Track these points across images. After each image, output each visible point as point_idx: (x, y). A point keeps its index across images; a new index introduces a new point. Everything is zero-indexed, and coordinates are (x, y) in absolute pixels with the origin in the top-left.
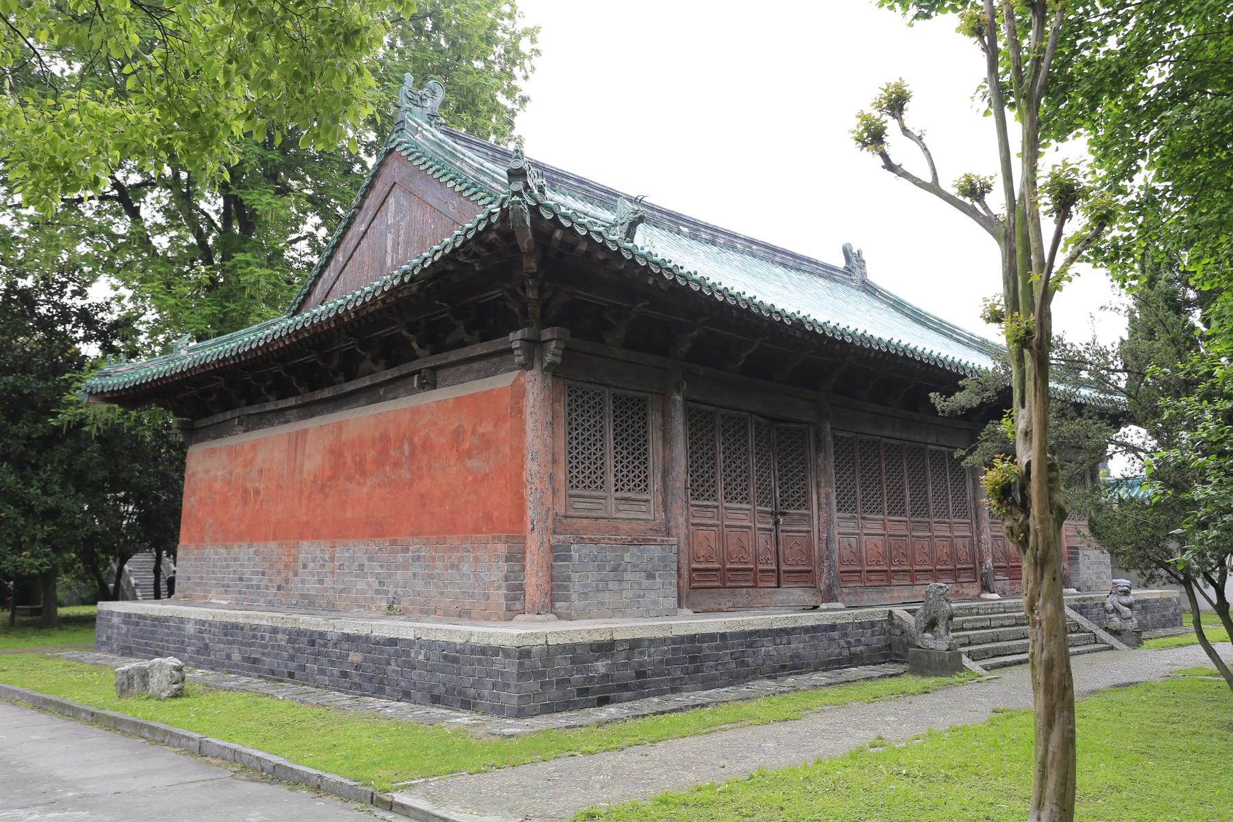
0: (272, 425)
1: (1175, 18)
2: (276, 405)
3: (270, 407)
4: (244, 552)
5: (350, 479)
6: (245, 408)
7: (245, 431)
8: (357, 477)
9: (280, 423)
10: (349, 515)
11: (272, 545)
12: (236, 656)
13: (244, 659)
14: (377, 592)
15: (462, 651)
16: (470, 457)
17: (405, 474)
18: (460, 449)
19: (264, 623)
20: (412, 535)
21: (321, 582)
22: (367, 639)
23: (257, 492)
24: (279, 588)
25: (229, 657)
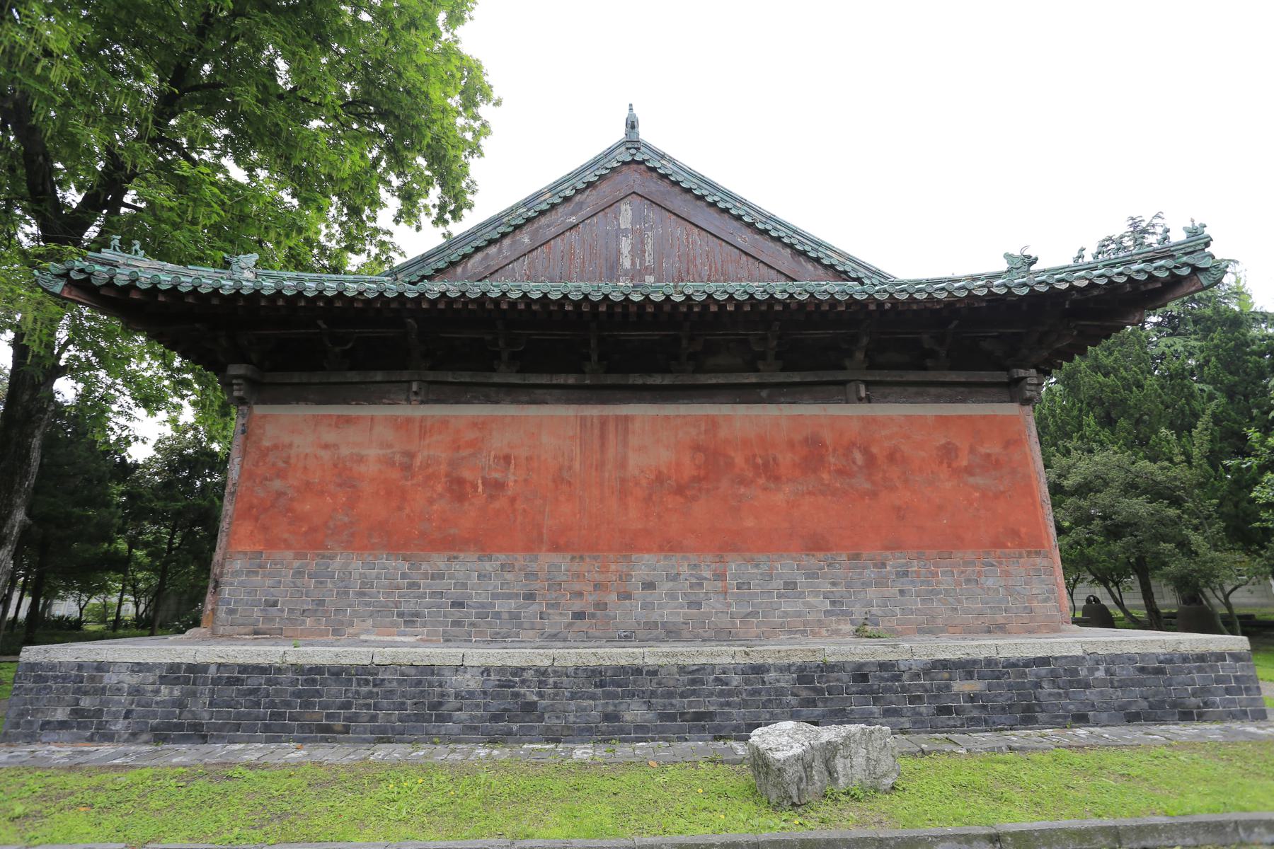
1: (349, 133)
3: (497, 379)
7: (422, 402)
15: (1170, 661)
16: (972, 474)
18: (954, 465)
22: (990, 662)
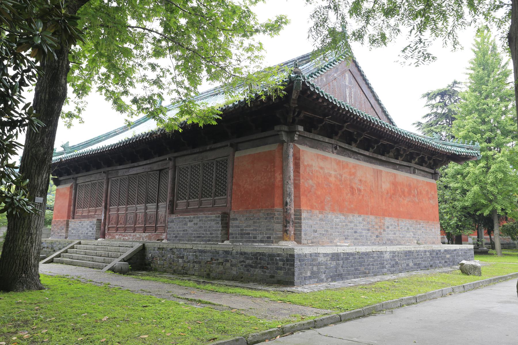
0: (351, 157)
2: (359, 150)
4: (357, 219)
5: (400, 196)
6: (425, 168)
8: (403, 196)
9: (354, 158)
10: (401, 209)
11: (372, 217)
12: (411, 264)
13: (415, 264)
19: (421, 249)
20: (420, 219)
21: (395, 234)
23: (360, 190)
24: (377, 236)
25: (408, 265)
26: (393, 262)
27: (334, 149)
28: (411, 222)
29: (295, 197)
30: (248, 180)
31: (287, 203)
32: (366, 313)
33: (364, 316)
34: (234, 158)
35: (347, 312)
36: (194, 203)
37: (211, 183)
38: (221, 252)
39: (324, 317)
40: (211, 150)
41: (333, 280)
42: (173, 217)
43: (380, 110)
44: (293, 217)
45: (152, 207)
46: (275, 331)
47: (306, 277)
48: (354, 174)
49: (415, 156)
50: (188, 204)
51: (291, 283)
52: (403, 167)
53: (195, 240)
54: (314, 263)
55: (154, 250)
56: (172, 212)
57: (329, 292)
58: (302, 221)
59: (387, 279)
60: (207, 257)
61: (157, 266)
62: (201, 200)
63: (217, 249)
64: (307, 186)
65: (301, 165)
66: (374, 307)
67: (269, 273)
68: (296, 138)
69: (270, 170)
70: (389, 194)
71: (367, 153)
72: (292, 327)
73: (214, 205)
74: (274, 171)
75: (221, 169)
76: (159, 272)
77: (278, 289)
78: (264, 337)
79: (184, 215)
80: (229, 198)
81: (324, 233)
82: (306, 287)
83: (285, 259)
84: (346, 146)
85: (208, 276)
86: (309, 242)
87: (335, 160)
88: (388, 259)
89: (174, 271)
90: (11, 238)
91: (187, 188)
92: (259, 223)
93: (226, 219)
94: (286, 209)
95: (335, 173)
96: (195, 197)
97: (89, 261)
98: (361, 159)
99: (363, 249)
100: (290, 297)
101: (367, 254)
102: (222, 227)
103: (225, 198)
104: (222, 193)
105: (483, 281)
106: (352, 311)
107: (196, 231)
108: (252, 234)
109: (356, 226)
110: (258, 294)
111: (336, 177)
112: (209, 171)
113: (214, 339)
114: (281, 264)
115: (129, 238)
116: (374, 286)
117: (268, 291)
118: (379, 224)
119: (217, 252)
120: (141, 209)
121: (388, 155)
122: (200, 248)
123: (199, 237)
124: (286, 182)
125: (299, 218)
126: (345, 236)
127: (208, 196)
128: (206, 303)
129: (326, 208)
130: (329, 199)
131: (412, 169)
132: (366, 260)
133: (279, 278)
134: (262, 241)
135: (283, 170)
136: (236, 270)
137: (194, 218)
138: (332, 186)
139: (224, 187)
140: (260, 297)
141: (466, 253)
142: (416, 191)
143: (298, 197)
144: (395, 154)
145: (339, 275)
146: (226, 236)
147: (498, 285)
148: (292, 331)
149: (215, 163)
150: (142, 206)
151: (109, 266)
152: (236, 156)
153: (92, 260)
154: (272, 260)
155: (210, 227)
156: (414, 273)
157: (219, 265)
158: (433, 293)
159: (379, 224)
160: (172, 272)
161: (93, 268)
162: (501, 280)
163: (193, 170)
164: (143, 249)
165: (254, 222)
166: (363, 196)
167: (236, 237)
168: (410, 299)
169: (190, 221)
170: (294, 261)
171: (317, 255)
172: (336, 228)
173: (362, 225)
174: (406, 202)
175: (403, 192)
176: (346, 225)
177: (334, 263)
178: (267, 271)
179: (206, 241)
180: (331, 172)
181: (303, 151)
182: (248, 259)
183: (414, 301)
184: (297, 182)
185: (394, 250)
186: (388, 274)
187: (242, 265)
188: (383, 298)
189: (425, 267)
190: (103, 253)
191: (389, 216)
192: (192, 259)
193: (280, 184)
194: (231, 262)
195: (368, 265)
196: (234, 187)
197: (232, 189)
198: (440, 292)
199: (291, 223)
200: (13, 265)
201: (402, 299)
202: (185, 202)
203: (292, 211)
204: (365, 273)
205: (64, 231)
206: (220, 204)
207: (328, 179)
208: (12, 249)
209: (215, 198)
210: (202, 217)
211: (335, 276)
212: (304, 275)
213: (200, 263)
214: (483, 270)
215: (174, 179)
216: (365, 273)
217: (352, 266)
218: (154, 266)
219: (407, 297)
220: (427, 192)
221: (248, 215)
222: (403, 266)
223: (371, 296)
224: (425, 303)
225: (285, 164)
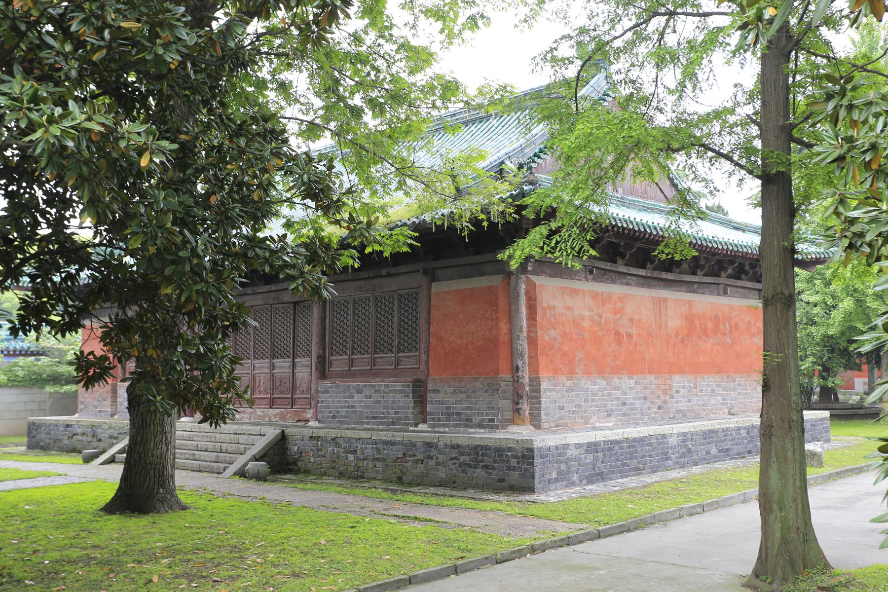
0: (615, 283)
2: (628, 270)
5: (700, 338)
8: (704, 337)
9: (621, 283)
10: (701, 359)
11: (651, 378)
12: (714, 451)
13: (720, 451)
14: (722, 404)
17: (728, 340)
19: (732, 425)
20: (735, 373)
21: (689, 401)
23: (630, 336)
24: (660, 408)
25: (708, 453)
26: (684, 450)
27: (588, 273)
28: (718, 378)
29: (530, 357)
30: (455, 331)
31: (518, 369)
32: (632, 527)
33: (629, 531)
34: (430, 292)
35: (607, 527)
36: (362, 361)
37: (390, 329)
38: (419, 445)
39: (579, 533)
40: (389, 275)
41: (590, 482)
42: (327, 384)
43: (668, 182)
44: (527, 388)
45: (283, 366)
46: (524, 549)
47: (551, 479)
48: (621, 311)
49: (725, 265)
50: (351, 363)
51: (531, 490)
52: (706, 285)
53: (368, 423)
54: (562, 458)
55: (302, 440)
56: (323, 375)
57: (584, 501)
58: (542, 394)
59: (670, 478)
60: (396, 452)
61: (309, 466)
62: (375, 358)
63: (414, 440)
64: (548, 339)
65: (538, 309)
66: (642, 519)
67: (497, 475)
68: (530, 268)
69: (490, 317)
70: (680, 337)
71: (642, 272)
72: (542, 545)
73: (398, 365)
74: (497, 319)
75: (406, 308)
76: (314, 475)
77: (512, 498)
78: (513, 556)
79: (348, 382)
80: (424, 357)
81: (574, 409)
82: (552, 493)
83: (520, 455)
84: (608, 266)
85: (400, 480)
86: (553, 425)
87: (590, 292)
88: (675, 446)
89: (341, 473)
90: (139, 439)
91: (348, 335)
92: (475, 398)
93: (420, 390)
94: (518, 377)
95: (590, 313)
96: (362, 352)
97: (187, 459)
98: (632, 282)
99: (634, 432)
100: (532, 509)
101: (640, 440)
102: (415, 402)
103: (416, 356)
104: (410, 347)
105: (817, 477)
106: (614, 525)
107: (370, 407)
108: (465, 414)
109: (625, 394)
110: (488, 506)
111: (592, 320)
112: (387, 309)
113: (462, 558)
114: (514, 462)
115: (243, 417)
116: (648, 490)
117: (498, 501)
118: (663, 387)
119: (413, 445)
120: (262, 368)
121: (678, 270)
122: (384, 438)
123: (375, 418)
124: (515, 336)
125: (536, 390)
126: (606, 411)
127: (385, 350)
128: (426, 520)
129: (578, 371)
130: (581, 356)
131: (721, 287)
132: (639, 449)
133: (512, 482)
134: (480, 426)
135: (511, 317)
136: (444, 471)
137: (365, 386)
138: (586, 334)
139: (414, 338)
140: (492, 511)
141: (814, 425)
142: (728, 325)
143: (534, 358)
144: (691, 265)
145: (597, 474)
146: (423, 416)
147: (840, 481)
148: (543, 548)
149: (396, 296)
150: (265, 363)
151: (233, 468)
152: (433, 291)
153: (192, 457)
154: (501, 456)
155: (393, 402)
156: (717, 465)
157: (417, 463)
158: (730, 498)
159: (663, 387)
160: (337, 474)
161: (200, 471)
162: (850, 474)
163: (357, 306)
164: (283, 438)
165: (468, 397)
166: (636, 344)
167: (439, 420)
168: (694, 507)
169: (358, 392)
170: (533, 457)
171: (566, 446)
172: (593, 400)
173: (635, 391)
174: (709, 346)
175: (705, 330)
176: (609, 394)
177: (590, 458)
178: (493, 472)
179: (387, 424)
180: (584, 313)
181: (540, 286)
182: (463, 454)
183: (699, 510)
184: (532, 334)
185: (685, 431)
186: (675, 469)
187: (454, 464)
188: (656, 507)
189: (739, 454)
190: (211, 446)
191: (679, 373)
192: (371, 454)
193: (506, 338)
194: (437, 459)
195: (643, 457)
196: (433, 340)
197: (428, 343)
198: (742, 497)
199: (525, 398)
200: (146, 477)
201: (683, 508)
202: (345, 359)
203: (526, 380)
204: (638, 469)
205: (108, 402)
206: (409, 365)
207: (580, 324)
208: (142, 455)
209: (399, 355)
210: (380, 386)
211: (592, 475)
212: (547, 476)
213: (384, 460)
214: (825, 459)
215: (323, 320)
216: (638, 469)
217: (618, 460)
218: (303, 466)
219: (691, 504)
220: (749, 323)
221: (457, 384)
222: (699, 455)
223: (642, 504)
224: (714, 513)
225: (513, 308)
